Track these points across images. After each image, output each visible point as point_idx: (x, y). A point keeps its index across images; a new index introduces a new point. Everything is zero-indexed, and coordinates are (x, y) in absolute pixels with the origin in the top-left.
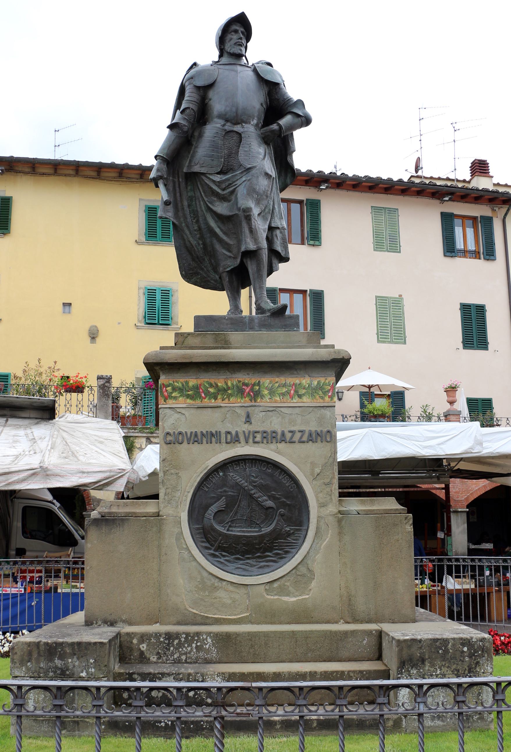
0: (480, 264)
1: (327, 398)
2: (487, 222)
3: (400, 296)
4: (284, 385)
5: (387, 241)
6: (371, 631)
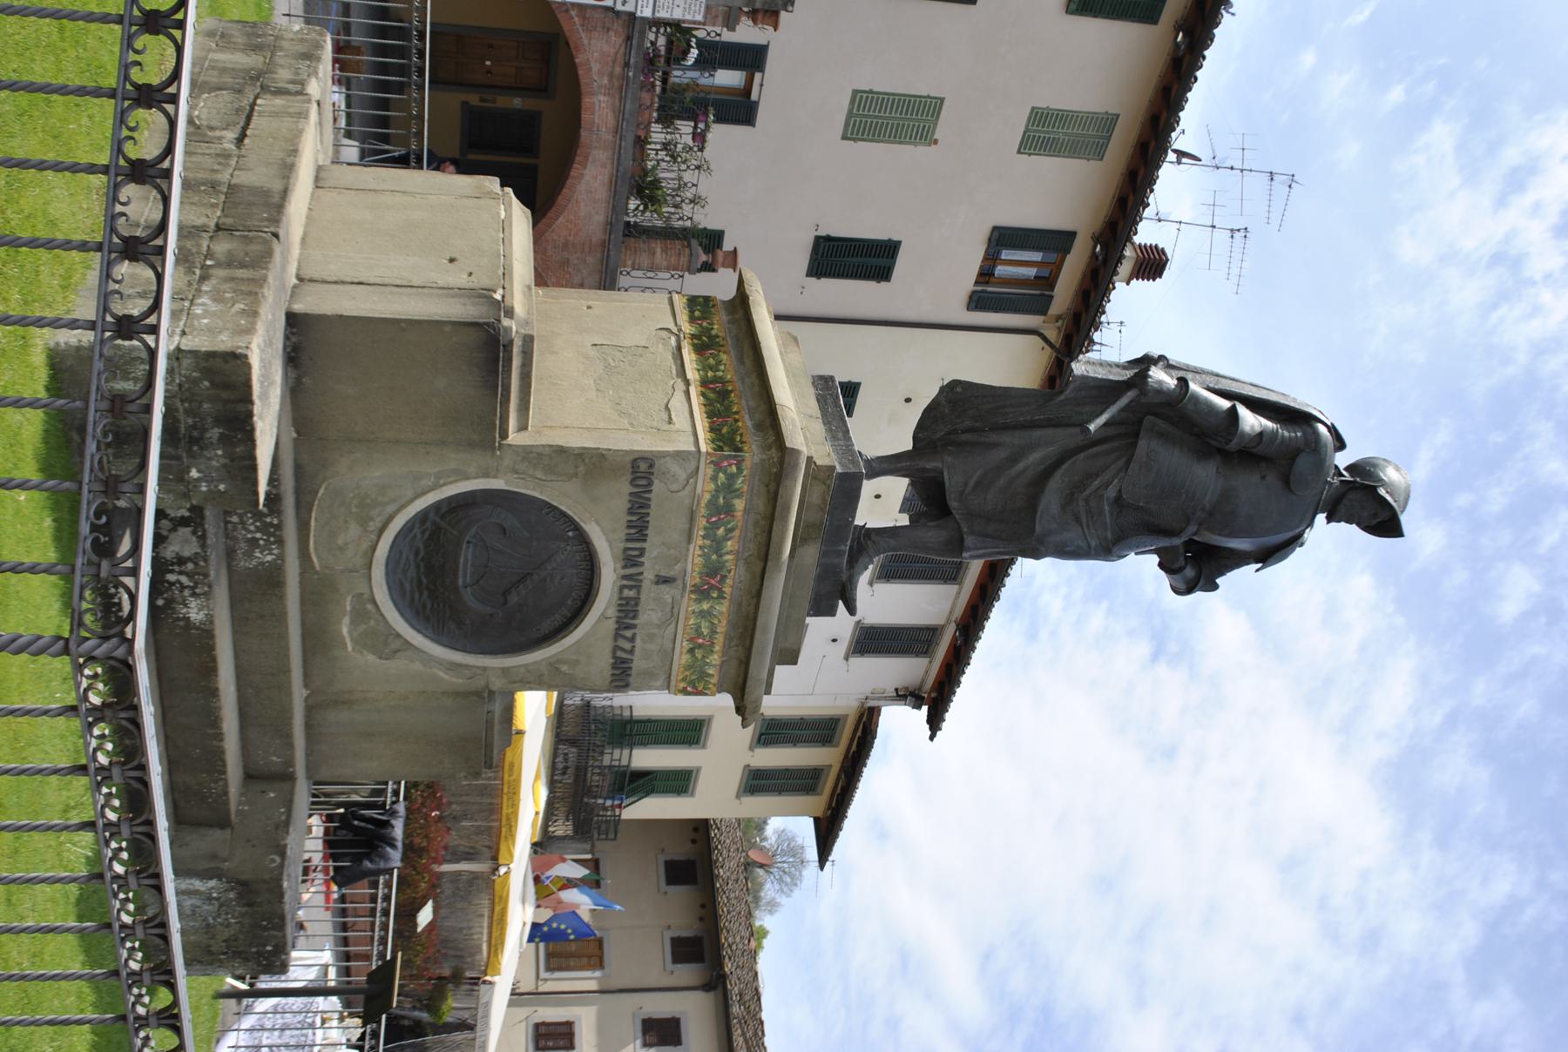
0: (967, 281)
1: (683, 685)
2: (1039, 306)
3: (936, 142)
4: (713, 632)
5: (1046, 133)
6: (293, 766)
